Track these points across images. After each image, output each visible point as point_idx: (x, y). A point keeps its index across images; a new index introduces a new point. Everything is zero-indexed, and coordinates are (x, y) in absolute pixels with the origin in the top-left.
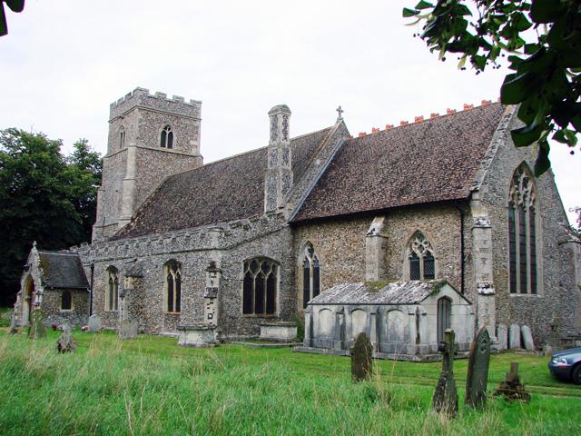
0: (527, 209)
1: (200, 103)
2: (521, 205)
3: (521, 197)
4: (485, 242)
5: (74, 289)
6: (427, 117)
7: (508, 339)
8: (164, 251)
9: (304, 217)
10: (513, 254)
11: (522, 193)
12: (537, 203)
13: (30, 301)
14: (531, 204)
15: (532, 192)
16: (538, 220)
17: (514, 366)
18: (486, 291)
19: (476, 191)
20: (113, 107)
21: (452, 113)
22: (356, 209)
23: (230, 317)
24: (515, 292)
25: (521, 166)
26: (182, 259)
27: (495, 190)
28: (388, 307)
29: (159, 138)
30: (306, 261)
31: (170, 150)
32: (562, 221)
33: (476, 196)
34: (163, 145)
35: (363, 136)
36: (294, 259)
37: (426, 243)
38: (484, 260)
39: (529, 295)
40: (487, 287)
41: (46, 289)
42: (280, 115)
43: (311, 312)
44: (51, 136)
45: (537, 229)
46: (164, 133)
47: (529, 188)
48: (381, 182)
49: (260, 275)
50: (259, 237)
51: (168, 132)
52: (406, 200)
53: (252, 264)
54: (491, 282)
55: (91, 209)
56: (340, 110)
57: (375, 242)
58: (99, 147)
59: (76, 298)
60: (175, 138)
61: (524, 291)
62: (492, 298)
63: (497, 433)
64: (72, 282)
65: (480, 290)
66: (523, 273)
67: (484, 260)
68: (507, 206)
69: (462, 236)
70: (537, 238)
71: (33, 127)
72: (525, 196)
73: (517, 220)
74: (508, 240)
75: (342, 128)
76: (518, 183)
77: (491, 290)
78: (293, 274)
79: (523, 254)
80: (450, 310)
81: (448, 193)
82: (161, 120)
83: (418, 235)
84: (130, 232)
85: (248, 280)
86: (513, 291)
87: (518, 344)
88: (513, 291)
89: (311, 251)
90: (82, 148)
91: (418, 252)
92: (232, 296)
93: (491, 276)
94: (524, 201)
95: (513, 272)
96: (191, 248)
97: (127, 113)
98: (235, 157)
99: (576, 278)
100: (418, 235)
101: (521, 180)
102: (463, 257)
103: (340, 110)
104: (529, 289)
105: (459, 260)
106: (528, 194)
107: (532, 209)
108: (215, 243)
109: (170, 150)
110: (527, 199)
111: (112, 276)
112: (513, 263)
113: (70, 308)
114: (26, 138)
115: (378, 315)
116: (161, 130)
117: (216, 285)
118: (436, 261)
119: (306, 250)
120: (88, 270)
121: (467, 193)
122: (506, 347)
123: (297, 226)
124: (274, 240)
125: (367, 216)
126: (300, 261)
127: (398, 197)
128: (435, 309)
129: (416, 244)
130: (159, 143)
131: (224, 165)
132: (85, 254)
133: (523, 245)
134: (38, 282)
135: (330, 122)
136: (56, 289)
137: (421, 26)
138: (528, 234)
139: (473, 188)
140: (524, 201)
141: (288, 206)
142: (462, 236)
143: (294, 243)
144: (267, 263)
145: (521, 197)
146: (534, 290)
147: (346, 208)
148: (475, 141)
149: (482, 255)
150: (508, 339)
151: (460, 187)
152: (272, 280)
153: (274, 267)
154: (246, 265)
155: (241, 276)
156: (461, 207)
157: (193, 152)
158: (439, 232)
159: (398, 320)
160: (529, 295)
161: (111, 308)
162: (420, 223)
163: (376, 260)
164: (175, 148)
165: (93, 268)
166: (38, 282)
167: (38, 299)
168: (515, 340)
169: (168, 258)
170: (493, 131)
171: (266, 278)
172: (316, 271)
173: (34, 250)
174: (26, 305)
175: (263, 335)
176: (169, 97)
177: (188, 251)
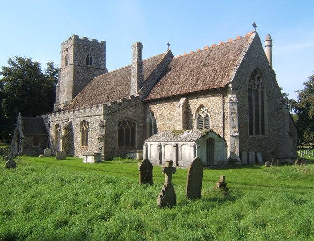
0: (259, 92)
1: (106, 42)
4: (234, 109)
7: (248, 159)
8: (80, 116)
10: (251, 115)
11: (257, 84)
12: (265, 89)
13: (18, 142)
14: (262, 89)
15: (262, 83)
16: (266, 97)
22: (173, 94)
23: (111, 148)
24: (258, 135)
26: (88, 120)
28: (166, 143)
30: (150, 120)
31: (92, 66)
34: (87, 64)
35: (302, 95)
36: (145, 119)
37: (206, 110)
38: (233, 119)
39: (260, 136)
40: (235, 132)
45: (265, 102)
46: (87, 58)
47: (261, 81)
48: (185, 80)
49: (127, 128)
51: (90, 57)
53: (122, 123)
56: (169, 45)
57: (180, 111)
58: (58, 65)
60: (93, 60)
61: (257, 134)
63: (130, 240)
66: (257, 124)
67: (233, 119)
68: (247, 90)
69: (223, 106)
70: (265, 107)
71: (26, 56)
72: (258, 86)
73: (253, 97)
74: (248, 108)
75: (170, 55)
76: (254, 79)
78: (145, 127)
80: (214, 144)
81: (216, 85)
85: (121, 130)
87: (254, 162)
88: (251, 134)
90: (51, 65)
91: (202, 115)
92: (112, 138)
93: (237, 127)
94: (258, 88)
95: (251, 124)
96: (93, 115)
98: (120, 70)
100: (201, 106)
101: (256, 77)
102: (224, 117)
103: (169, 45)
104: (260, 134)
105: (222, 119)
109: (92, 66)
111: (84, 126)
112: (251, 120)
114: (21, 60)
118: (210, 119)
119: (150, 115)
122: (246, 163)
125: (176, 98)
126: (148, 119)
127: (193, 87)
129: (201, 111)
133: (257, 110)
134: (21, 133)
138: (260, 105)
139: (228, 82)
140: (258, 88)
142: (223, 106)
145: (256, 86)
146: (263, 134)
147: (168, 94)
148: (232, 57)
149: (233, 116)
150: (248, 159)
151: (222, 82)
152: (133, 130)
154: (119, 123)
155: (117, 128)
159: (186, 150)
163: (181, 119)
166: (21, 133)
167: (21, 141)
168: (252, 158)
170: (241, 52)
171: (130, 129)
173: (19, 117)
174: (16, 144)
177: (91, 116)
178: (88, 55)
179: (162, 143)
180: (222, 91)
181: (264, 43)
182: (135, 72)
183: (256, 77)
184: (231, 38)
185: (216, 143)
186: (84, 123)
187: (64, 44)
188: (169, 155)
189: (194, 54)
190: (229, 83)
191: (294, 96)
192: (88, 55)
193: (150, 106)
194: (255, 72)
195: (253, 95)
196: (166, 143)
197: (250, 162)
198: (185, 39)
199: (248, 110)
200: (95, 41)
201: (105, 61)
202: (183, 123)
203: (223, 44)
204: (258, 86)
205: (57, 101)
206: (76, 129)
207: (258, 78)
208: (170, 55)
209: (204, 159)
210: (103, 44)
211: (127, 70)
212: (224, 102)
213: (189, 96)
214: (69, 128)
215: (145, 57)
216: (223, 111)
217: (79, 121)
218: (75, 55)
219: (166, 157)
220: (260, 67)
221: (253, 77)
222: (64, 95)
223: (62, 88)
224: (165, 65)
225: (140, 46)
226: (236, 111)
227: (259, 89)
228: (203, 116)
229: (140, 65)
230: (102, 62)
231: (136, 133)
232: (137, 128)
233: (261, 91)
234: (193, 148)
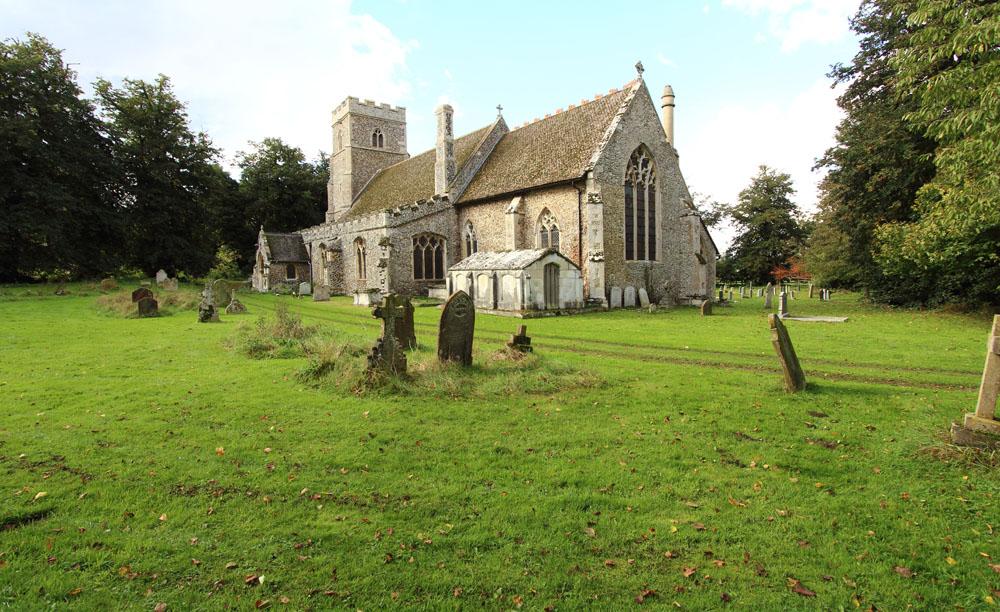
2: (641, 183)
3: (640, 176)
4: (596, 216)
5: (297, 263)
7: (623, 299)
9: (464, 199)
10: (629, 226)
16: (658, 197)
17: (524, 328)
19: (590, 171)
22: (500, 191)
25: (640, 148)
26: (364, 235)
27: (610, 170)
28: (479, 272)
30: (468, 236)
31: (381, 149)
32: (684, 197)
33: (591, 175)
34: (375, 144)
36: (459, 234)
39: (647, 261)
40: (597, 255)
41: (272, 263)
42: (164, 82)
46: (375, 135)
47: (650, 168)
49: (428, 248)
51: (378, 135)
52: (539, 182)
53: (420, 240)
54: (601, 250)
55: (325, 196)
57: (511, 219)
59: (298, 270)
60: (384, 140)
61: (641, 257)
62: (602, 264)
64: (294, 256)
68: (623, 183)
72: (644, 176)
75: (501, 124)
76: (637, 164)
77: (601, 257)
78: (459, 247)
79: (641, 226)
80: (558, 274)
83: (546, 211)
84: (344, 219)
85: (417, 252)
88: (630, 256)
89: (471, 227)
92: (403, 265)
94: (644, 179)
98: (425, 154)
99: (695, 245)
100: (546, 211)
102: (581, 229)
104: (647, 257)
107: (652, 188)
110: (647, 178)
112: (629, 235)
113: (294, 277)
116: (372, 133)
120: (308, 247)
121: (582, 173)
124: (442, 219)
125: (507, 197)
126: (464, 237)
128: (541, 274)
131: (418, 158)
132: (313, 236)
137: (844, 87)
139: (587, 168)
140: (644, 179)
141: (452, 191)
143: (458, 221)
144: (434, 238)
145: (640, 176)
146: (652, 257)
149: (594, 227)
152: (439, 252)
153: (441, 242)
154: (415, 241)
155: (412, 248)
157: (402, 151)
161: (361, 277)
164: (385, 148)
165: (311, 246)
168: (630, 300)
169: (356, 235)
172: (475, 243)
173: (262, 232)
175: (430, 295)
178: (374, 129)
179: (498, 272)
180: (578, 184)
181: (658, 102)
182: (441, 158)
184: (598, 94)
185: (561, 272)
186: (359, 240)
187: (335, 112)
188: (484, 291)
189: (539, 124)
190: (590, 171)
192: (374, 129)
194: (641, 149)
196: (479, 272)
197: (626, 305)
198: (527, 98)
202: (516, 239)
203: (587, 104)
204: (644, 176)
205: (330, 208)
206: (349, 249)
207: (645, 164)
208: (501, 124)
209: (540, 299)
210: (401, 111)
211: (432, 153)
212: (580, 203)
213: (523, 193)
214: (337, 251)
215: (457, 134)
216: (580, 218)
217: (351, 238)
218: (354, 130)
219: (481, 295)
220: (647, 144)
221: (634, 159)
222: (339, 196)
223: (336, 186)
224: (497, 143)
225: (448, 112)
226: (600, 217)
227: (647, 181)
228: (548, 228)
229: (450, 146)
231: (819, 318)
233: (650, 186)
234: (518, 280)
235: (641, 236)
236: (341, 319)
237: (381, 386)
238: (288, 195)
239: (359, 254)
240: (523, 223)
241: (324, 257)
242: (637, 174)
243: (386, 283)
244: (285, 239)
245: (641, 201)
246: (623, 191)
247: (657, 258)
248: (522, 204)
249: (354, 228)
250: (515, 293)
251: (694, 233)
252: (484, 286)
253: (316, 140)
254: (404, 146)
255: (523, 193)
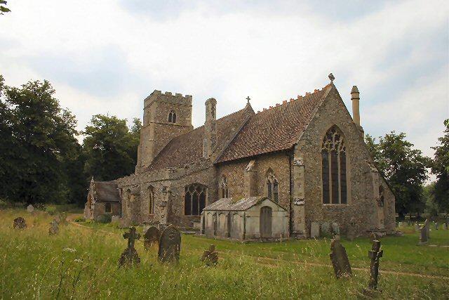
6: (288, 101)
10: (325, 180)
11: (334, 144)
12: (347, 149)
15: (343, 142)
18: (299, 203)
20: (146, 100)
21: (300, 97)
26: (154, 185)
28: (233, 212)
29: (168, 117)
33: (296, 147)
34: (170, 121)
35: (440, 153)
36: (217, 184)
38: (299, 185)
43: (204, 214)
44: (120, 117)
46: (171, 114)
47: (341, 141)
49: (195, 194)
50: (195, 172)
53: (191, 187)
55: (135, 157)
56: (248, 99)
57: (247, 175)
59: (114, 206)
65: (295, 203)
67: (299, 185)
72: (336, 146)
77: (301, 202)
79: (335, 180)
82: (168, 107)
83: (270, 170)
84: (149, 169)
85: (188, 196)
86: (326, 201)
88: (326, 201)
89: (225, 179)
93: (303, 194)
97: (151, 104)
100: (270, 170)
101: (334, 136)
103: (248, 99)
106: (340, 145)
107: (343, 154)
108: (167, 177)
110: (339, 147)
114: (104, 119)
115: (229, 217)
117: (167, 200)
123: (218, 166)
124: (205, 174)
125: (247, 160)
130: (168, 120)
132: (125, 182)
135: (242, 106)
136: (103, 201)
141: (214, 155)
144: (199, 187)
145: (334, 146)
146: (344, 201)
153: (204, 189)
154: (186, 189)
156: (289, 153)
157: (188, 124)
158: (280, 166)
160: (340, 205)
162: (271, 164)
165: (122, 190)
167: (93, 207)
172: (227, 190)
173: (92, 181)
176: (163, 92)
182: (208, 130)
183: (334, 136)
191: (430, 154)
193: (433, 158)
194: (334, 129)
195: (330, 157)
199: (321, 174)
200: (179, 96)
201: (190, 117)
207: (337, 138)
214: (137, 194)
221: (328, 135)
230: (198, 119)
232: (207, 195)
235: (335, 187)
236: (148, 205)
237: (431, 220)
238: (113, 150)
239: (150, 197)
240: (256, 178)
241: (129, 198)
242: (331, 145)
243: (165, 218)
244: (106, 184)
245: (334, 163)
246: (320, 158)
247: (348, 202)
248: (255, 166)
249: (149, 178)
250: (240, 227)
251: (374, 184)
252: (223, 220)
253: (129, 111)
254: (190, 121)
255: (256, 158)
